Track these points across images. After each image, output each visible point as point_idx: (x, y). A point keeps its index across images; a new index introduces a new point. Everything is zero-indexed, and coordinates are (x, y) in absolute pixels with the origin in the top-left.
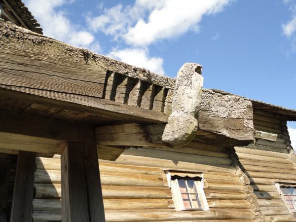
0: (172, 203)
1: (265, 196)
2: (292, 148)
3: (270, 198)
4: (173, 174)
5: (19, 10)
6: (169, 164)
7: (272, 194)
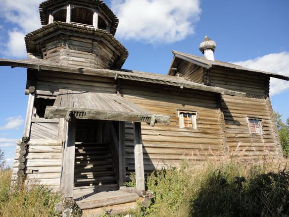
0: (179, 124)
1: (236, 123)
2: (269, 96)
3: (239, 125)
4: (181, 112)
5: (106, 11)
6: (180, 106)
7: (241, 123)
